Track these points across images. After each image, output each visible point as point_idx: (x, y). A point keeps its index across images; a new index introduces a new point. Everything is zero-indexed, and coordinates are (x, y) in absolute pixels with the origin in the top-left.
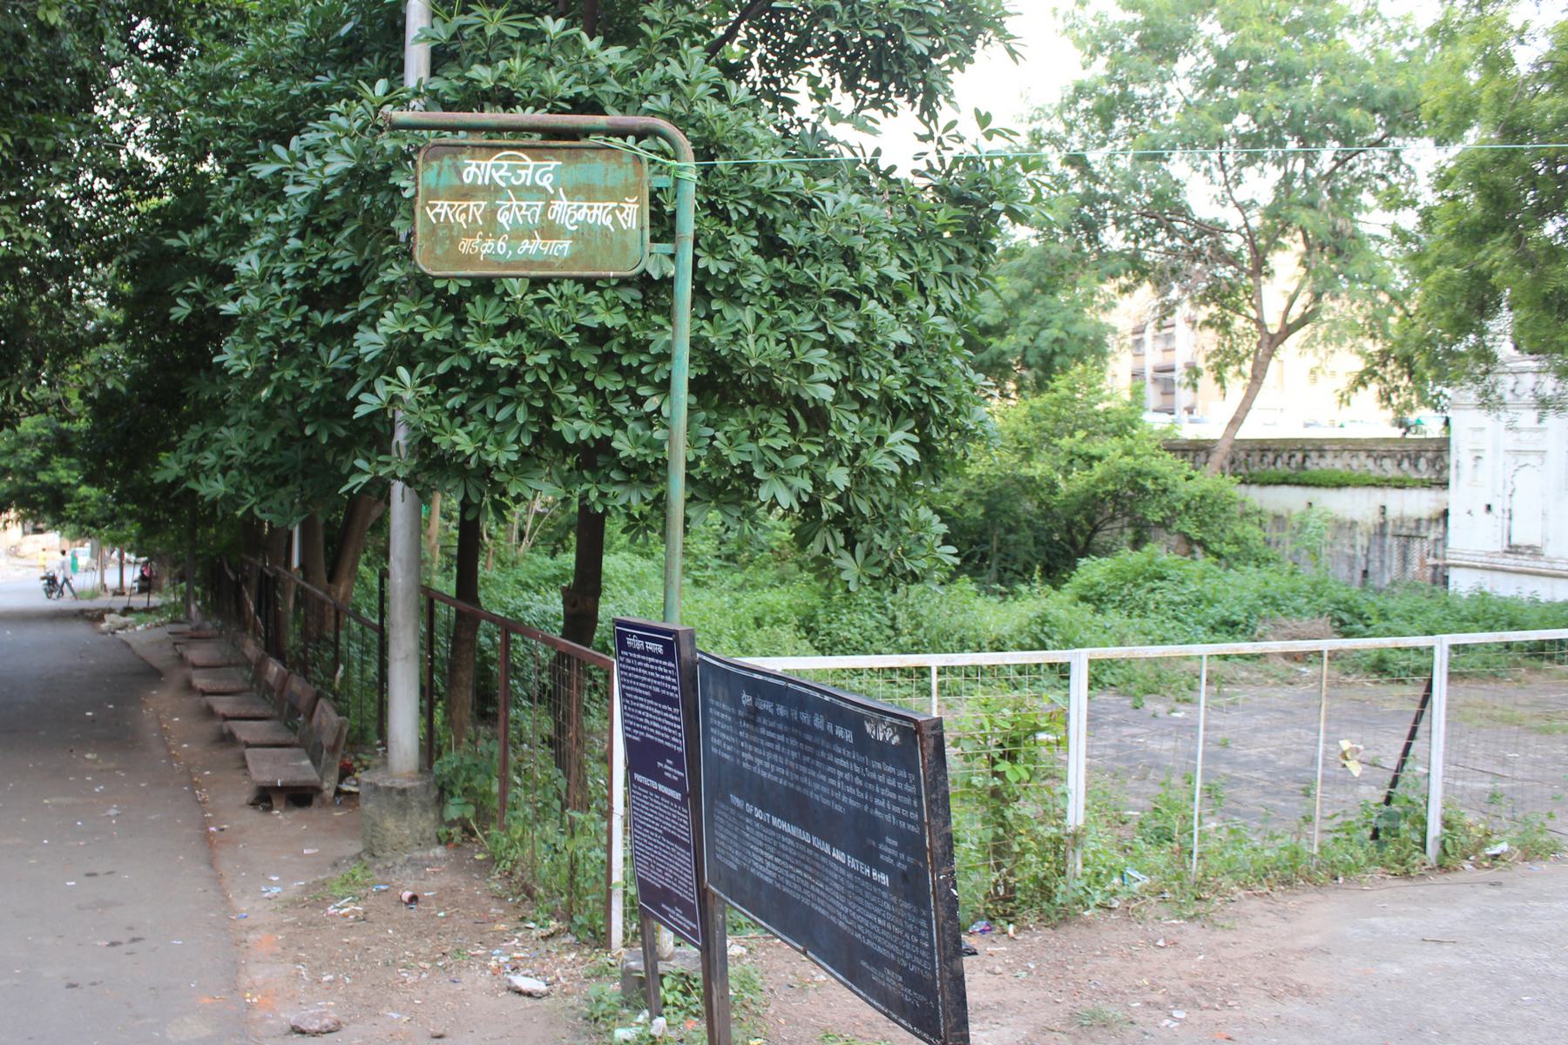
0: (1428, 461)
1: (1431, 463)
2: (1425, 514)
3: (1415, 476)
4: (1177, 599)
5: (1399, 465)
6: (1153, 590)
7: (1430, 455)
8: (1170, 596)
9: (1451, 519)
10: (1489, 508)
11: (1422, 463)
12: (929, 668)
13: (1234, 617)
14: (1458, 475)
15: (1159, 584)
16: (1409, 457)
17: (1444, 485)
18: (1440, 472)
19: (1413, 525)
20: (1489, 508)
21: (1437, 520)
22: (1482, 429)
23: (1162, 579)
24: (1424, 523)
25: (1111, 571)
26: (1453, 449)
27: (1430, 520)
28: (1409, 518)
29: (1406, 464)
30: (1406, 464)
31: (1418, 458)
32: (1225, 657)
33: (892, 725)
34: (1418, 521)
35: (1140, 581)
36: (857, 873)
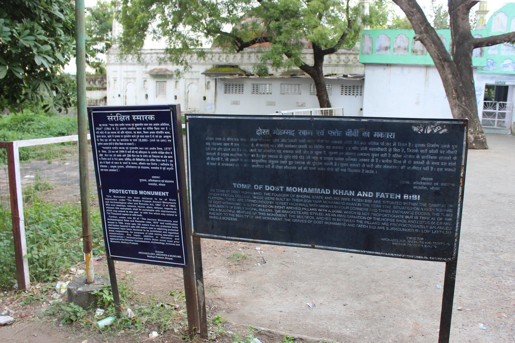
0: (99, 82)
1: (100, 82)
2: (99, 98)
3: (95, 86)
4: (40, 127)
5: (89, 83)
6: (30, 125)
7: (99, 80)
8: (38, 126)
9: (108, 100)
10: (119, 95)
11: (97, 82)
12: (506, 101)
13: (63, 132)
14: (109, 86)
15: (32, 122)
16: (92, 80)
17: (105, 89)
18: (103, 85)
19: (95, 102)
20: (119, 95)
21: (103, 100)
22: (116, 71)
23: (33, 121)
24: (98, 101)
25: (12, 119)
26: (107, 78)
27: (100, 100)
28: (94, 100)
29: (91, 83)
30: (91, 83)
31: (95, 81)
32: (63, 144)
33: (441, 125)
34: (97, 101)
35: (24, 122)
36: (275, 192)
